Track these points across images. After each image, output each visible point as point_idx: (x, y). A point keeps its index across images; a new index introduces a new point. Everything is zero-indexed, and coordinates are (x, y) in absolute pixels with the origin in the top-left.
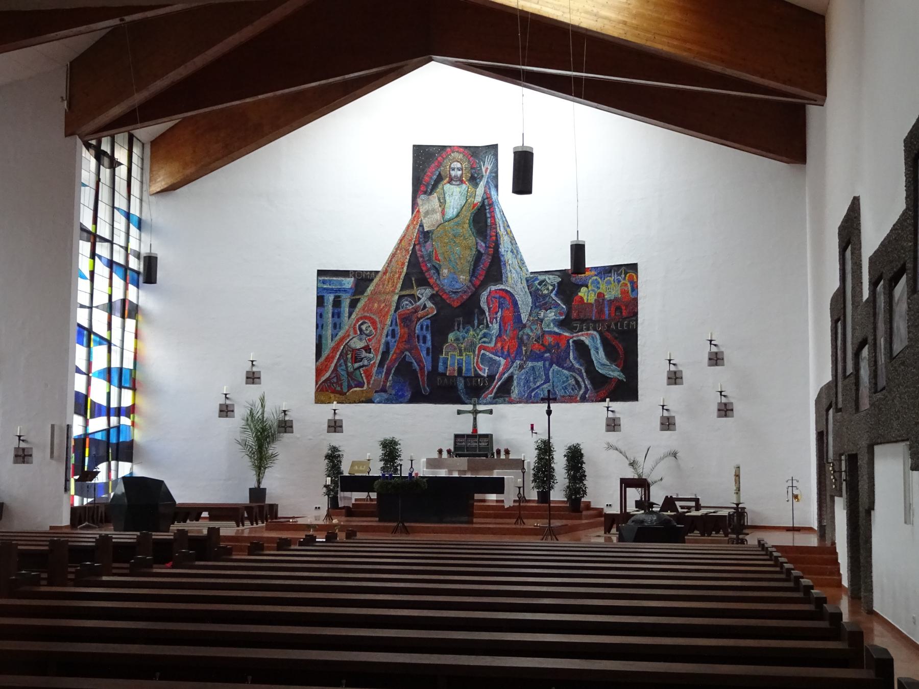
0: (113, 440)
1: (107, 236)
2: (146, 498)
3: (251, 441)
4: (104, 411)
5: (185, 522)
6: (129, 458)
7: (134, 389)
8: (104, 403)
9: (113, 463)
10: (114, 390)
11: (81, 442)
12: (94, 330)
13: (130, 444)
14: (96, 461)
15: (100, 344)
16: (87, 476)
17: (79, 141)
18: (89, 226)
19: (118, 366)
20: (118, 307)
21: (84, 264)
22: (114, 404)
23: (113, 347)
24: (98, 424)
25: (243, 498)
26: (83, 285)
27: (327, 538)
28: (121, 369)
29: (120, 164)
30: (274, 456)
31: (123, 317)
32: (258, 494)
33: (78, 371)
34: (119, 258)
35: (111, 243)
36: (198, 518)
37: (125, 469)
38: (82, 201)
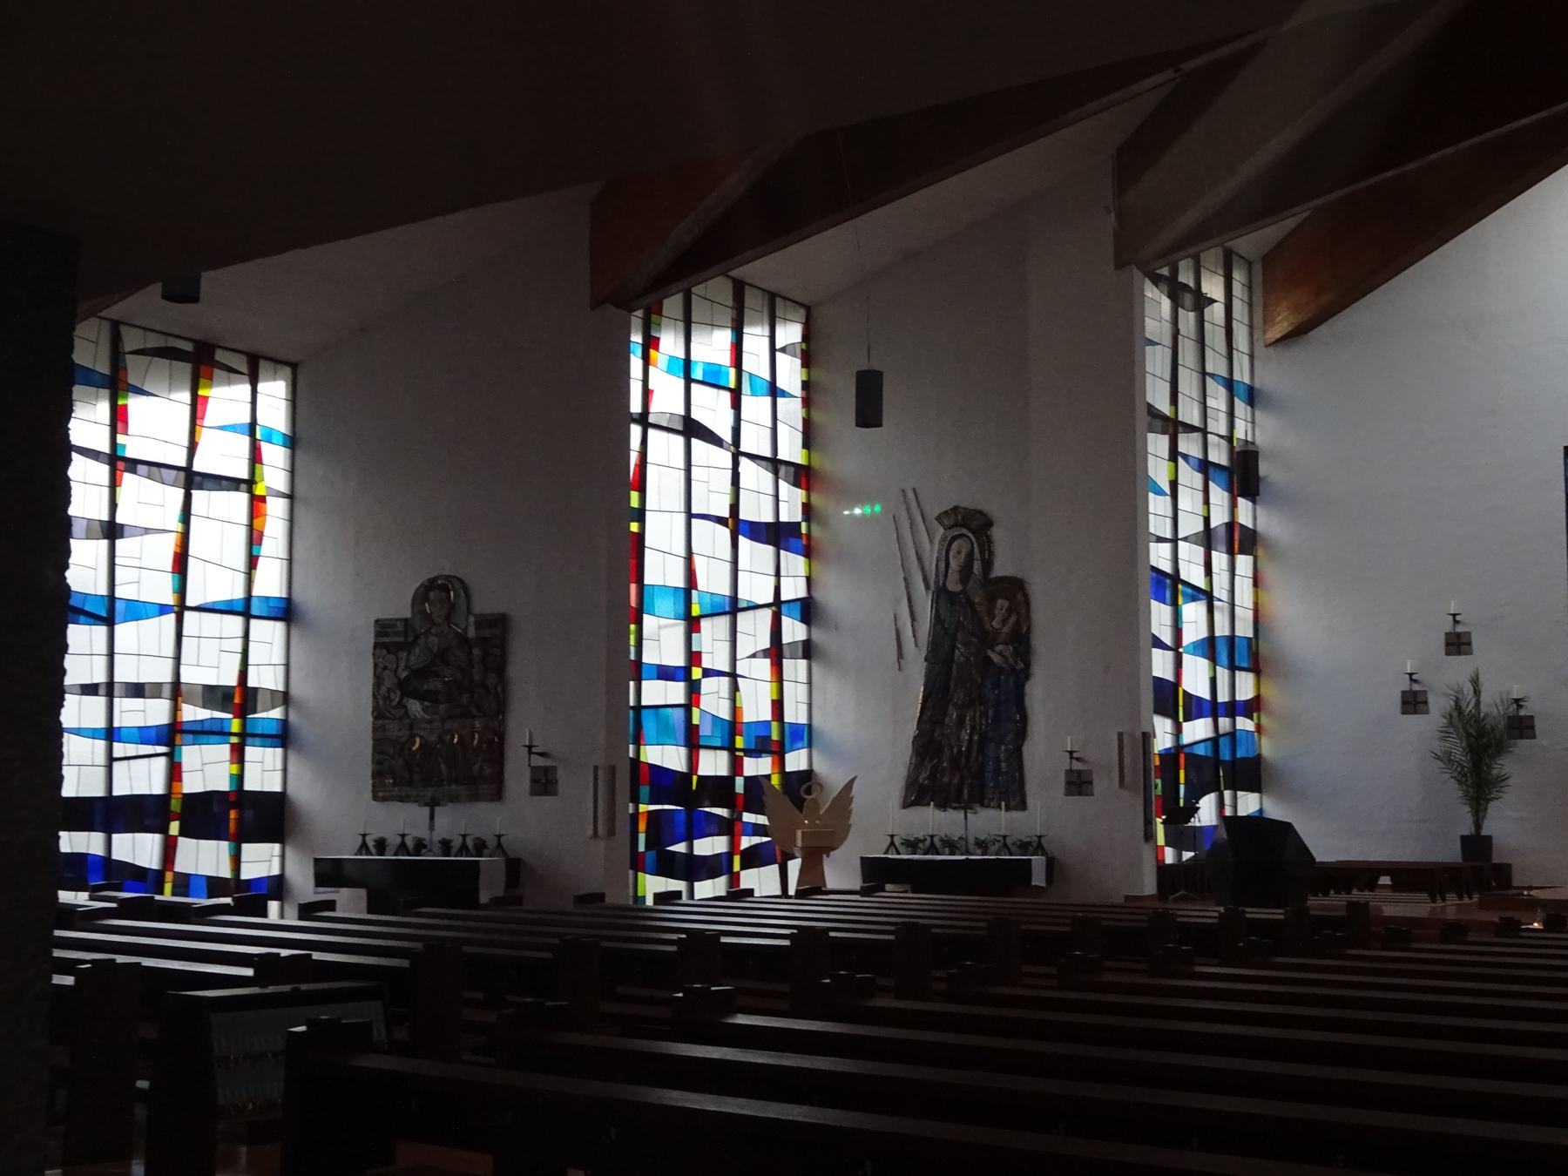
0: (1225, 755)
1: (1195, 420)
2: (1262, 851)
3: (1459, 753)
4: (1207, 708)
5: (1326, 894)
6: (1255, 786)
7: (1256, 669)
8: (1206, 695)
9: (1227, 794)
10: (1223, 674)
11: (1171, 758)
12: (1183, 577)
13: (1256, 762)
14: (1196, 793)
15: (1194, 599)
16: (1179, 816)
17: (1138, 274)
18: (1164, 407)
19: (1227, 633)
20: (1221, 535)
21: (1159, 470)
22: (1223, 697)
23: (1216, 603)
24: (1197, 730)
25: (1450, 853)
26: (1158, 506)
27: (1545, 922)
28: (1232, 639)
29: (1213, 301)
30: (1502, 779)
31: (1231, 553)
32: (1476, 845)
33: (1158, 643)
34: (1219, 455)
35: (1204, 432)
36: (1373, 886)
37: (1248, 803)
38: (1149, 368)
